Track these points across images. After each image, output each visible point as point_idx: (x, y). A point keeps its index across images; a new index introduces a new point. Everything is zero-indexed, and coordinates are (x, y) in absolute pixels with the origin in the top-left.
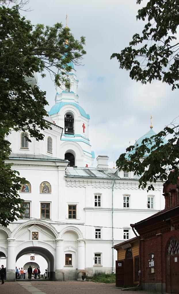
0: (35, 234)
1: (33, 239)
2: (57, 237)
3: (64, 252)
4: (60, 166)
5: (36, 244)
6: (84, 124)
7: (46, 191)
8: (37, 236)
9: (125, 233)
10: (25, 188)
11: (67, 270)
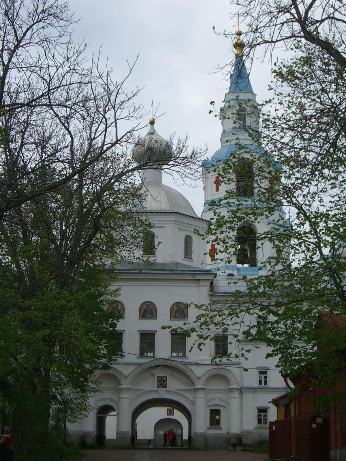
0: (162, 379)
1: (158, 387)
2: (195, 384)
3: (208, 406)
4: (201, 279)
5: (163, 394)
7: (179, 317)
8: (165, 382)
9: (261, 375)
10: (148, 312)
11: (212, 433)
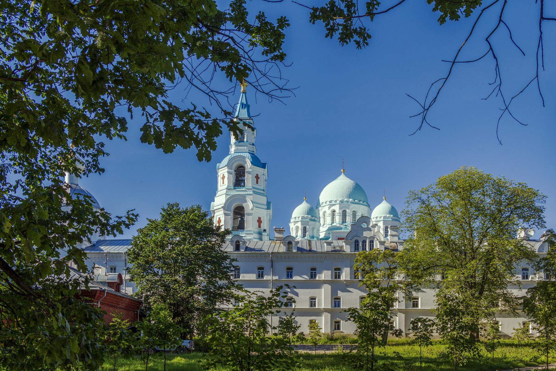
6: (257, 175)
9: (259, 270)
